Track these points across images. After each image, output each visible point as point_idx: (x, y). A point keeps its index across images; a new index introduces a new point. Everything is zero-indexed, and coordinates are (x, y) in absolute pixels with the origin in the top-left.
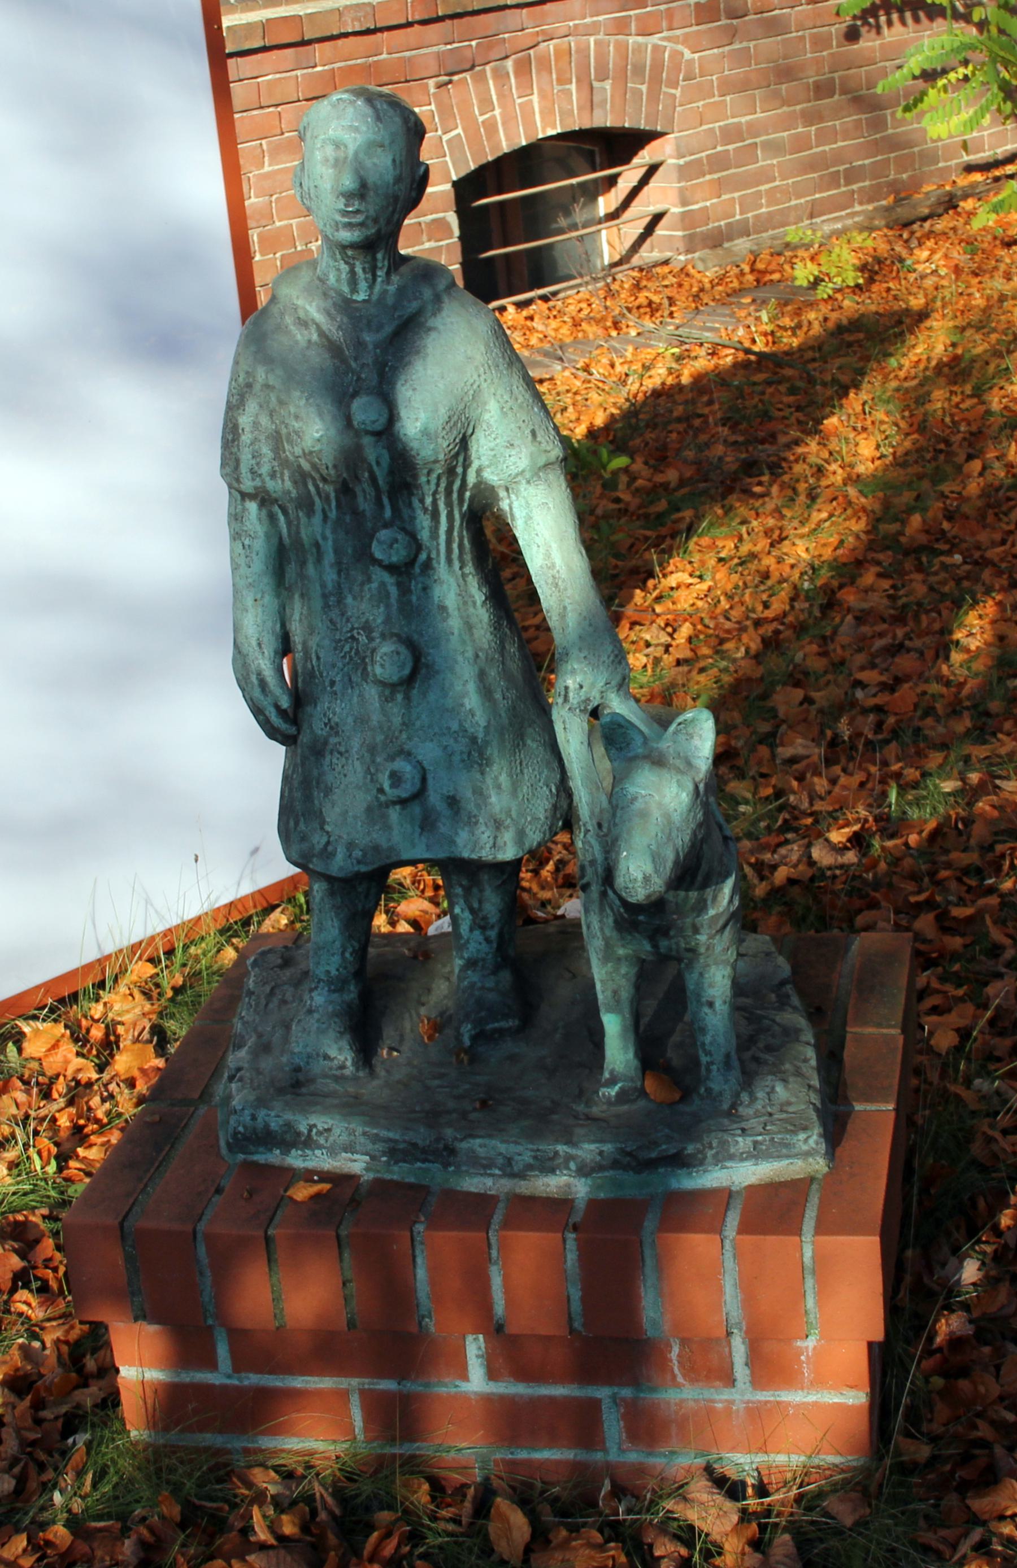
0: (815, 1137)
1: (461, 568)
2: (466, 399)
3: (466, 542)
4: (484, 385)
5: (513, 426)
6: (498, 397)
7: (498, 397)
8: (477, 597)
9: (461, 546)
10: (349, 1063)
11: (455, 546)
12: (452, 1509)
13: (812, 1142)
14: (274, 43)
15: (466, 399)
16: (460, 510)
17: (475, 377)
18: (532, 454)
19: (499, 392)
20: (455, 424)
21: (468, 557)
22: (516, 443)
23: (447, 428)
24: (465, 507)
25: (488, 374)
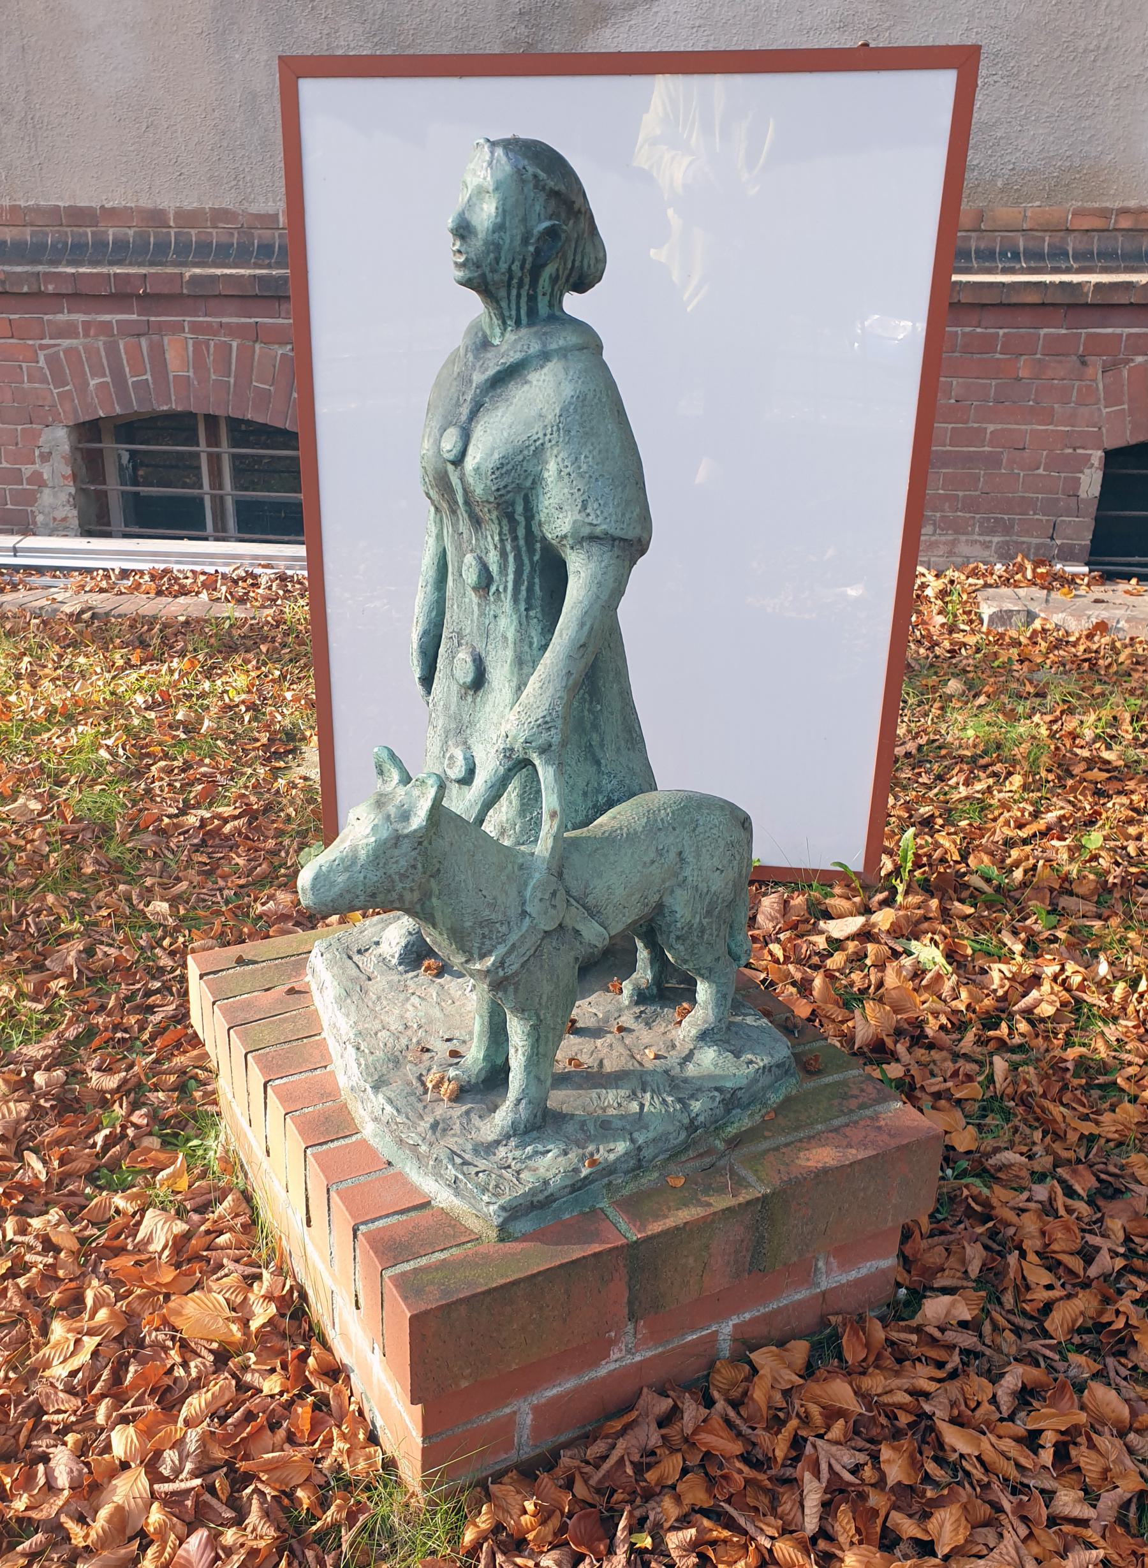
0: (496, 1207)
1: (526, 609)
2: (526, 452)
3: (537, 588)
4: (548, 445)
5: (566, 490)
6: (559, 459)
7: (559, 459)
8: (535, 640)
9: (530, 590)
10: (809, 1164)
11: (524, 588)
12: (272, 1264)
13: (492, 1208)
14: (696, 83)
15: (526, 452)
16: (531, 560)
17: (540, 435)
18: (575, 522)
19: (561, 455)
20: (508, 472)
21: (537, 603)
22: (566, 508)
23: (498, 473)
24: (536, 558)
25: (555, 435)
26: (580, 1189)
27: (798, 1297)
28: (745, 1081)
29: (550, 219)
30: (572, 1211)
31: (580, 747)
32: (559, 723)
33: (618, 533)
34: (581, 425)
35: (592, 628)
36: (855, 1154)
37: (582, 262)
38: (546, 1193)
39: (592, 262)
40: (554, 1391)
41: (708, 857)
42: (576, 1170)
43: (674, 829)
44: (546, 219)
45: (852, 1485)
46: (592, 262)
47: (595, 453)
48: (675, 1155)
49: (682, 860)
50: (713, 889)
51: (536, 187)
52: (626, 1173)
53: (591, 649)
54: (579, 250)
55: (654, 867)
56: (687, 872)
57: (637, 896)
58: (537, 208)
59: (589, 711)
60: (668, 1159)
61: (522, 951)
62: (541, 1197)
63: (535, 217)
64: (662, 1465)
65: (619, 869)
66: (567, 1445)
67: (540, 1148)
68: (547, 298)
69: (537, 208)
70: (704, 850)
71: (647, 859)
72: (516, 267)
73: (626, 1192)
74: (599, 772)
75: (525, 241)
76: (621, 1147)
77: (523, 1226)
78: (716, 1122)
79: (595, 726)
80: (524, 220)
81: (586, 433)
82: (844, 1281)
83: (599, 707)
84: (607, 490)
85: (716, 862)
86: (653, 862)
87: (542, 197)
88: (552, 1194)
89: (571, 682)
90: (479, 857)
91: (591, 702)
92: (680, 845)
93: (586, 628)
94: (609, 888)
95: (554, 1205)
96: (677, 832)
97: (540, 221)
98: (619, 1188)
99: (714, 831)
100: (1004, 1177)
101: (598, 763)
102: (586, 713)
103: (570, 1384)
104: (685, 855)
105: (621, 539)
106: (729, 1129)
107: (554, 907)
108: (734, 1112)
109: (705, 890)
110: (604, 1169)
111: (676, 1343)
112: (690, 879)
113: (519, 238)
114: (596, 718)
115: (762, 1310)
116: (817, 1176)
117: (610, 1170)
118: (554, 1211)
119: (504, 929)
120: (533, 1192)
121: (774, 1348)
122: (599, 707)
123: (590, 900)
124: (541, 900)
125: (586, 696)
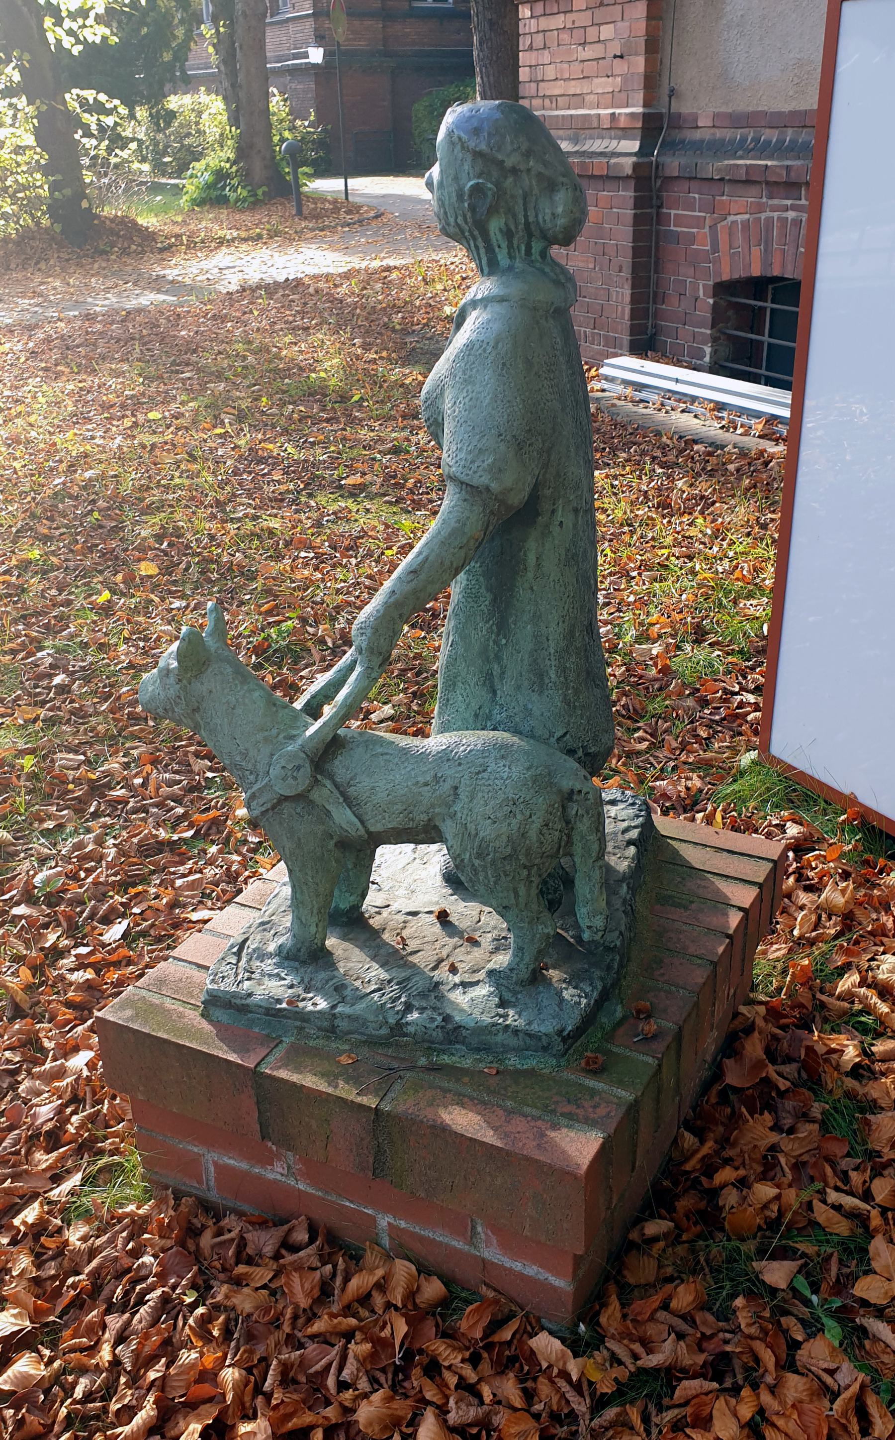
26: (273, 1016)
27: (454, 1243)
28: (473, 1024)
29: (479, 178)
30: (263, 1029)
31: (481, 672)
32: (369, 631)
33: (464, 478)
34: (464, 373)
35: (427, 558)
36: (489, 1137)
37: (537, 216)
38: (243, 1002)
39: (547, 218)
40: (231, 1162)
41: (482, 802)
42: (279, 1001)
43: (460, 764)
44: (474, 177)
45: (328, 1390)
46: (547, 218)
47: (467, 400)
48: (372, 1042)
49: (456, 795)
50: (481, 834)
51: (463, 148)
52: (320, 1029)
53: (423, 576)
54: (531, 205)
55: (426, 788)
56: (457, 807)
57: (400, 807)
58: (466, 167)
59: (495, 642)
60: (365, 1042)
61: (261, 801)
62: (238, 1001)
63: (464, 176)
64: (258, 1269)
65: (391, 777)
66: (240, 1214)
67: (283, 975)
68: (505, 251)
69: (466, 167)
70: (480, 795)
71: (421, 780)
72: (460, 220)
73: (311, 1043)
74: (493, 701)
75: (460, 196)
76: (322, 1004)
77: (219, 1014)
78: (433, 1043)
79: (498, 658)
80: (456, 178)
81: (465, 381)
82: (508, 1265)
83: (504, 641)
84: (466, 436)
85: (489, 810)
86: (426, 784)
87: (469, 157)
88: (248, 1005)
89: (392, 600)
90: (238, 711)
91: (498, 635)
92: (457, 781)
93: (421, 557)
94: (373, 788)
95: (250, 1015)
96: (460, 768)
97: (470, 180)
98: (308, 1037)
99: (497, 782)
100: (868, 1347)
101: (494, 692)
102: (491, 643)
103: (532, 1270)
104: (459, 791)
105: (467, 485)
106: (446, 1057)
107: (295, 778)
108: (458, 1046)
109: (473, 832)
110: (296, 1012)
111: (333, 1198)
112: (459, 815)
113: (454, 194)
114: (500, 650)
115: (417, 1230)
116: (433, 1127)
117: (304, 1017)
118: (248, 1019)
119: (252, 778)
120: (235, 995)
121: (413, 1268)
122: (504, 641)
123: (351, 791)
124: (283, 767)
125: (494, 627)
